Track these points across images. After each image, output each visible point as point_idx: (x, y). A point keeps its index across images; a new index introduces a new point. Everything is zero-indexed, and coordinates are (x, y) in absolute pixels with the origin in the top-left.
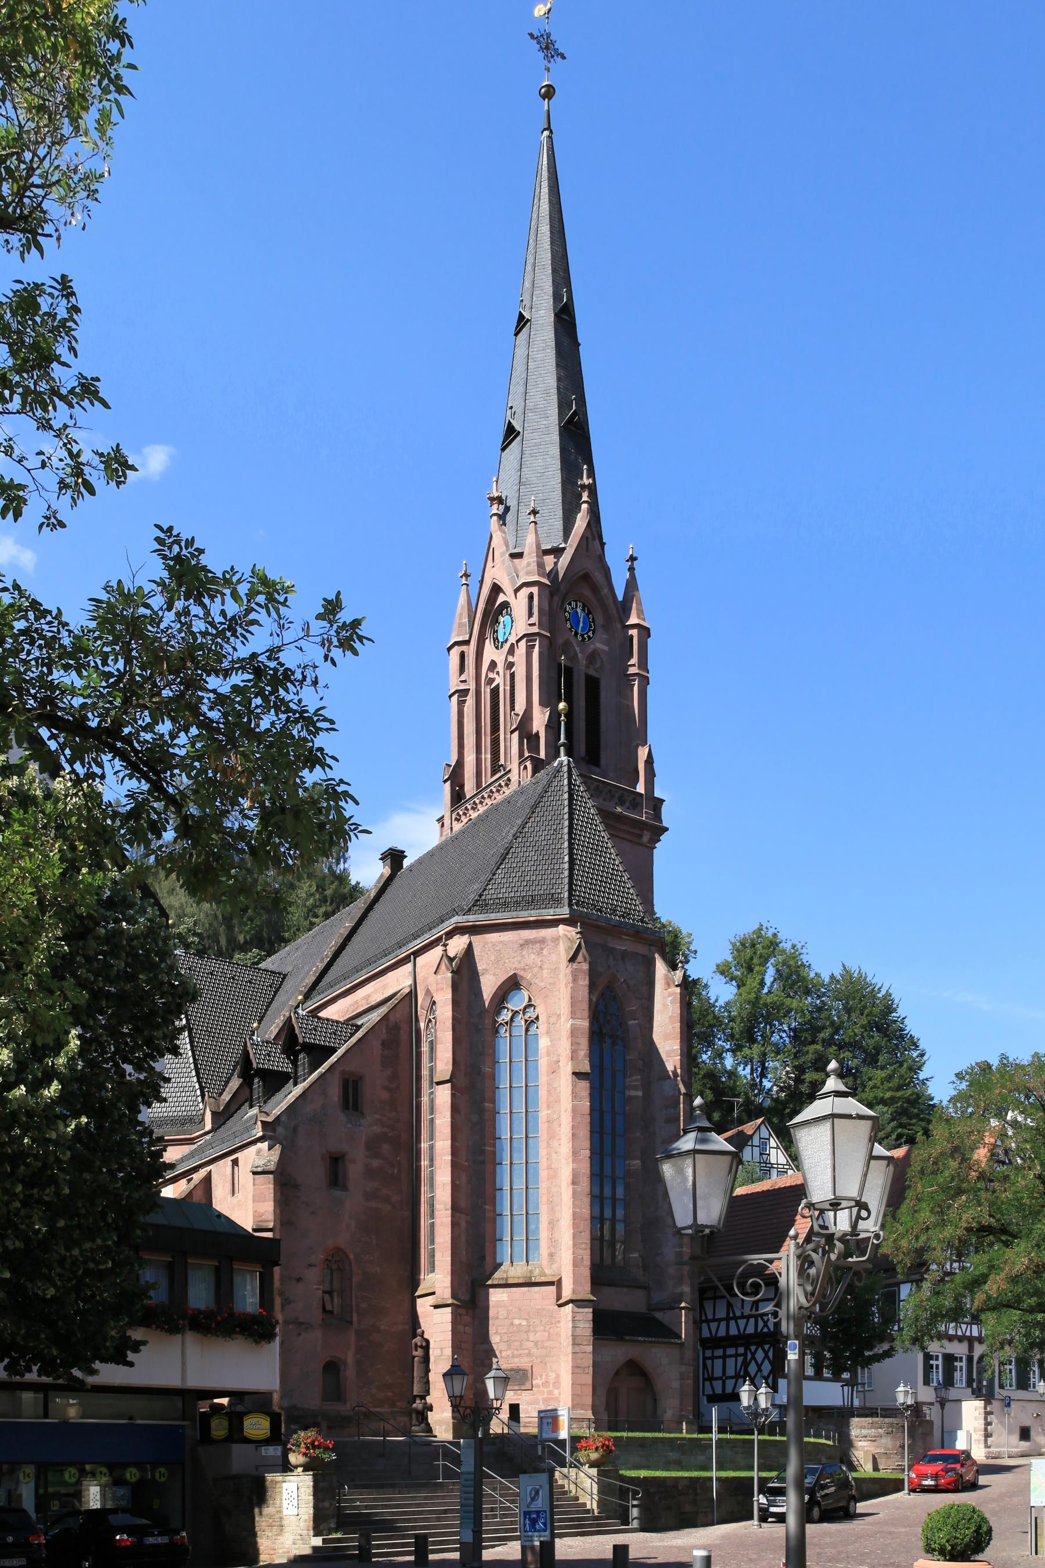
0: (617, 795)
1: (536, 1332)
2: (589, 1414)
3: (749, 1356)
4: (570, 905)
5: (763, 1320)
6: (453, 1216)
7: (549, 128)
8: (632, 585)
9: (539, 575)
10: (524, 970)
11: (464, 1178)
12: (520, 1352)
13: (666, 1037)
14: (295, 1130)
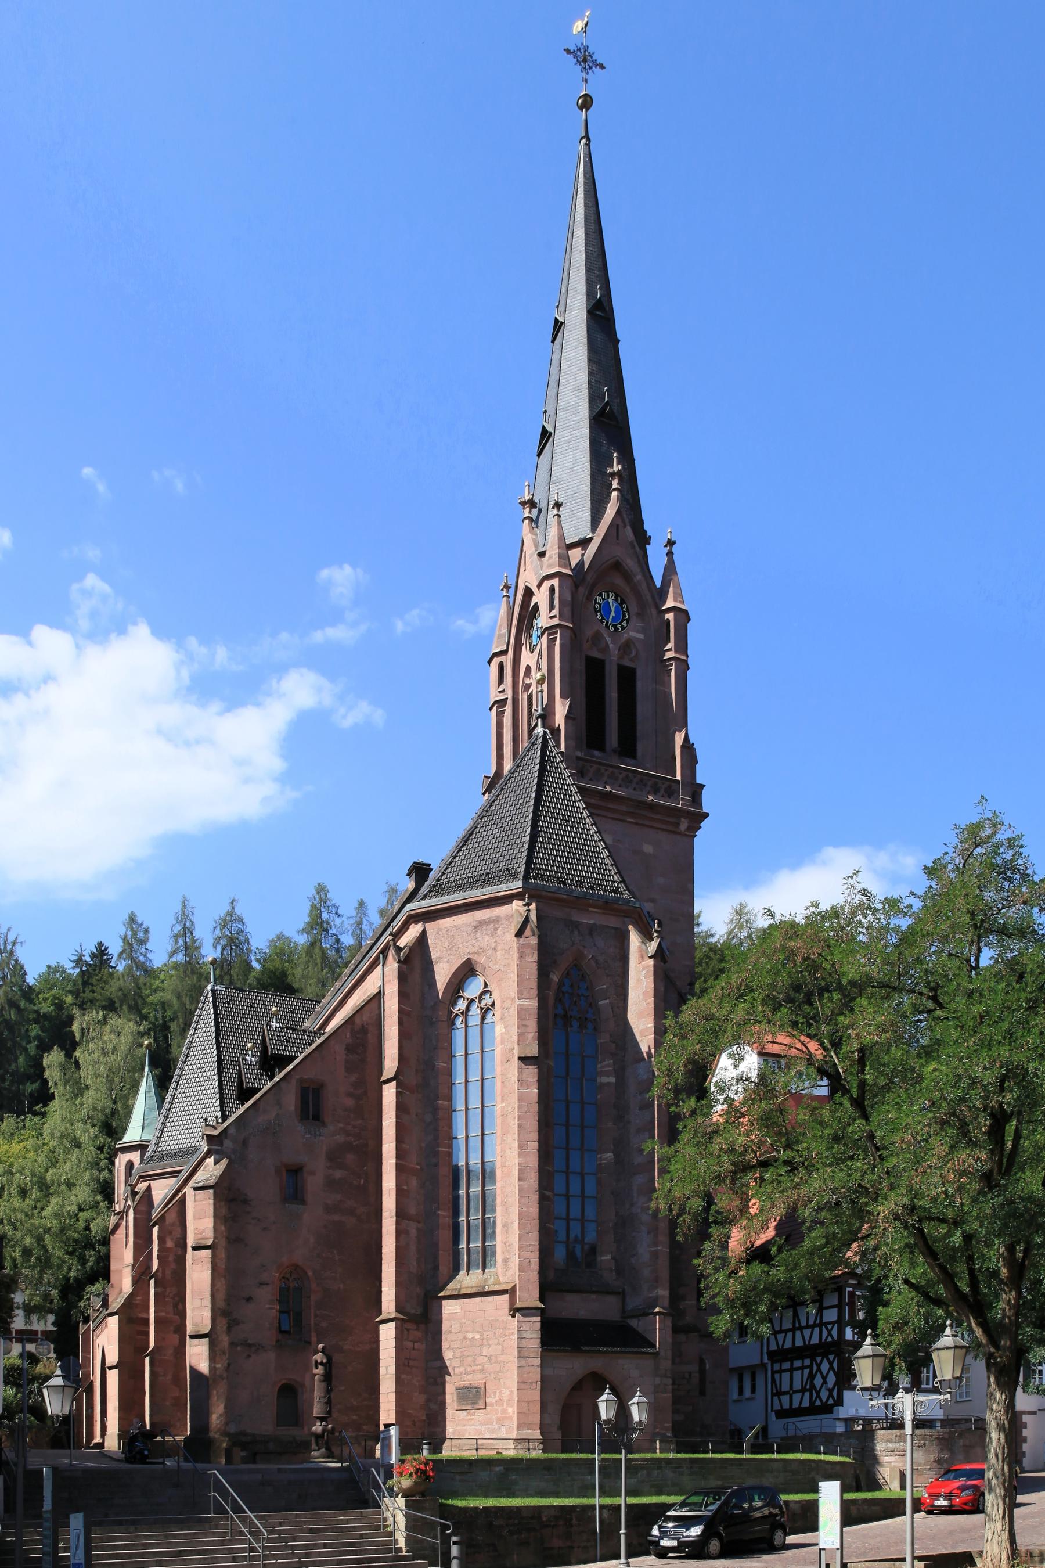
0: (650, 783)
1: (489, 1345)
2: (537, 1434)
3: (815, 1368)
4: (526, 878)
5: (827, 1328)
6: (397, 1223)
7: (587, 137)
8: (670, 569)
9: (560, 566)
10: (478, 953)
11: (414, 1182)
12: (474, 1368)
13: (640, 1015)
14: (245, 1143)
